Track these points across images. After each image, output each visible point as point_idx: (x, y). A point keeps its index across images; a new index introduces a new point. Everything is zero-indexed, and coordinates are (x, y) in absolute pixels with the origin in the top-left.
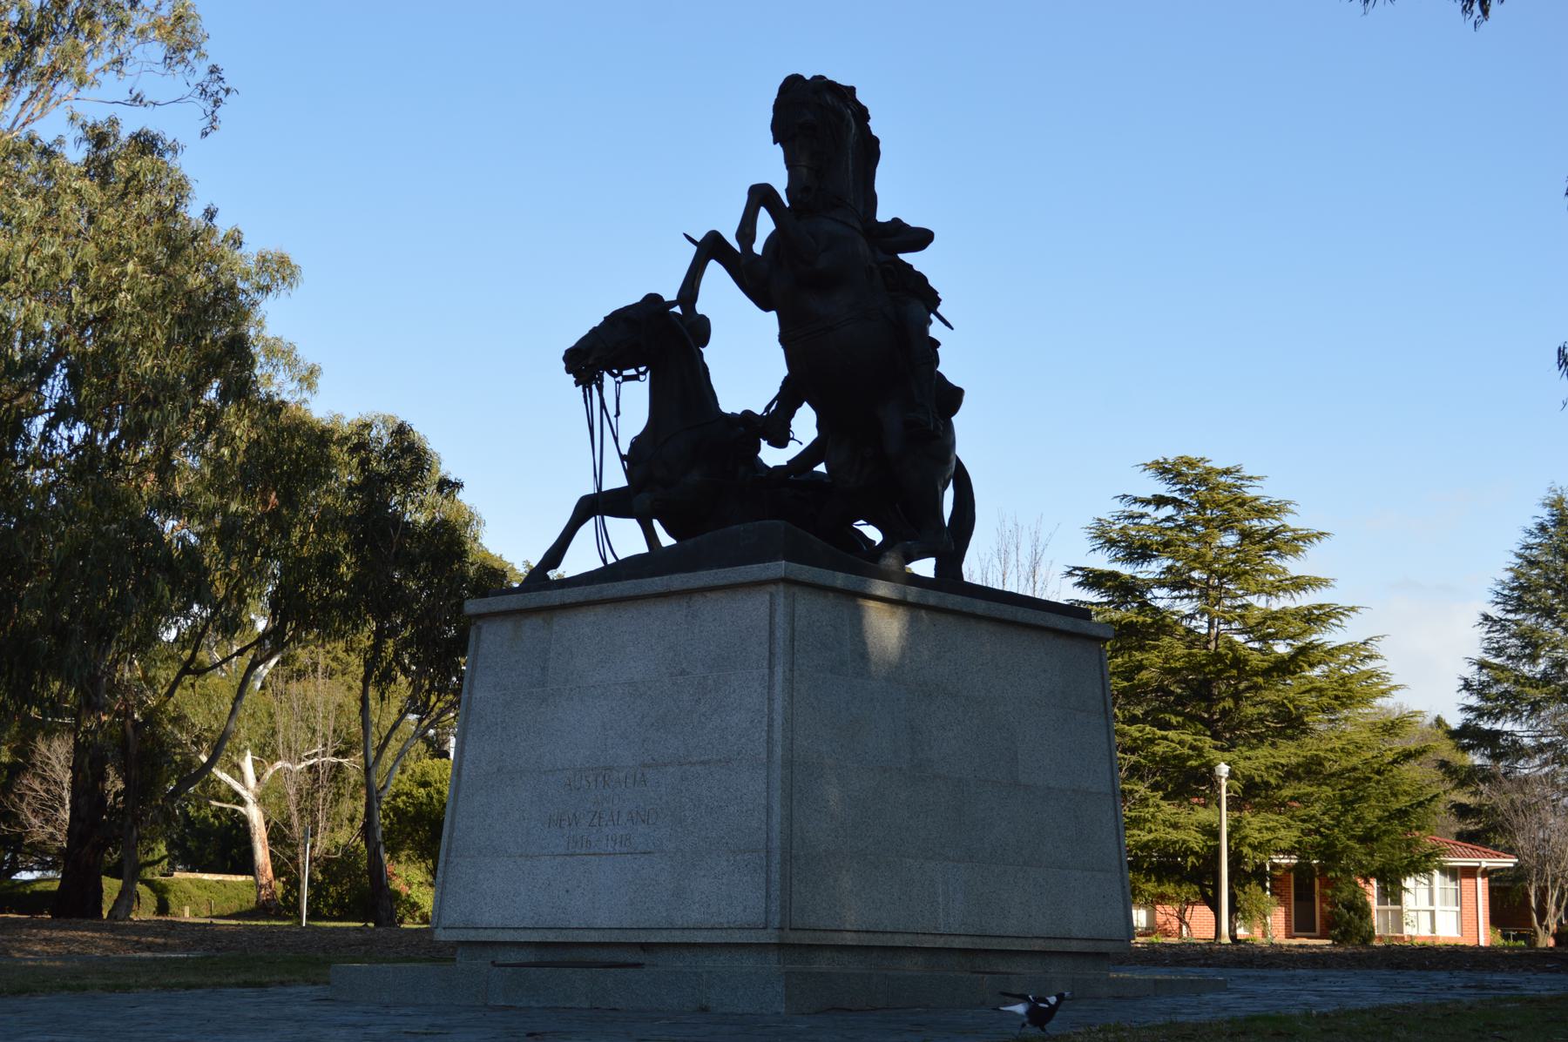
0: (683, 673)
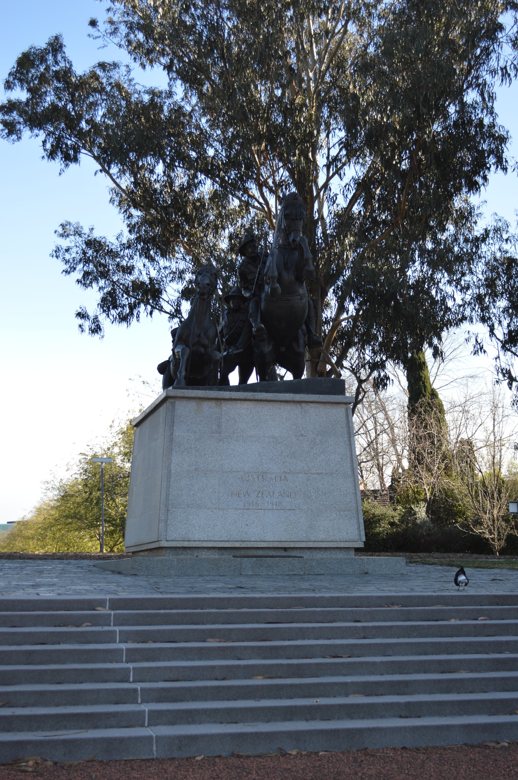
0: (302, 435)
